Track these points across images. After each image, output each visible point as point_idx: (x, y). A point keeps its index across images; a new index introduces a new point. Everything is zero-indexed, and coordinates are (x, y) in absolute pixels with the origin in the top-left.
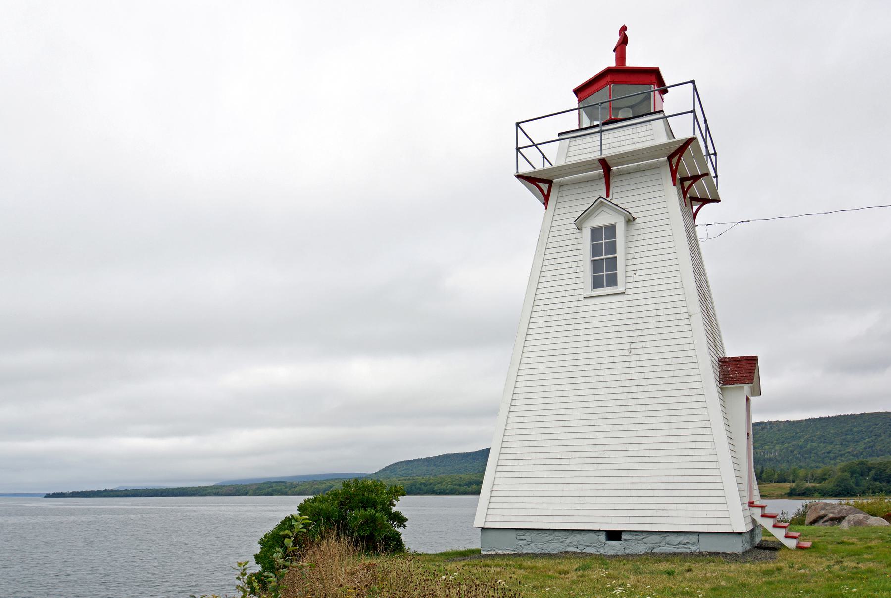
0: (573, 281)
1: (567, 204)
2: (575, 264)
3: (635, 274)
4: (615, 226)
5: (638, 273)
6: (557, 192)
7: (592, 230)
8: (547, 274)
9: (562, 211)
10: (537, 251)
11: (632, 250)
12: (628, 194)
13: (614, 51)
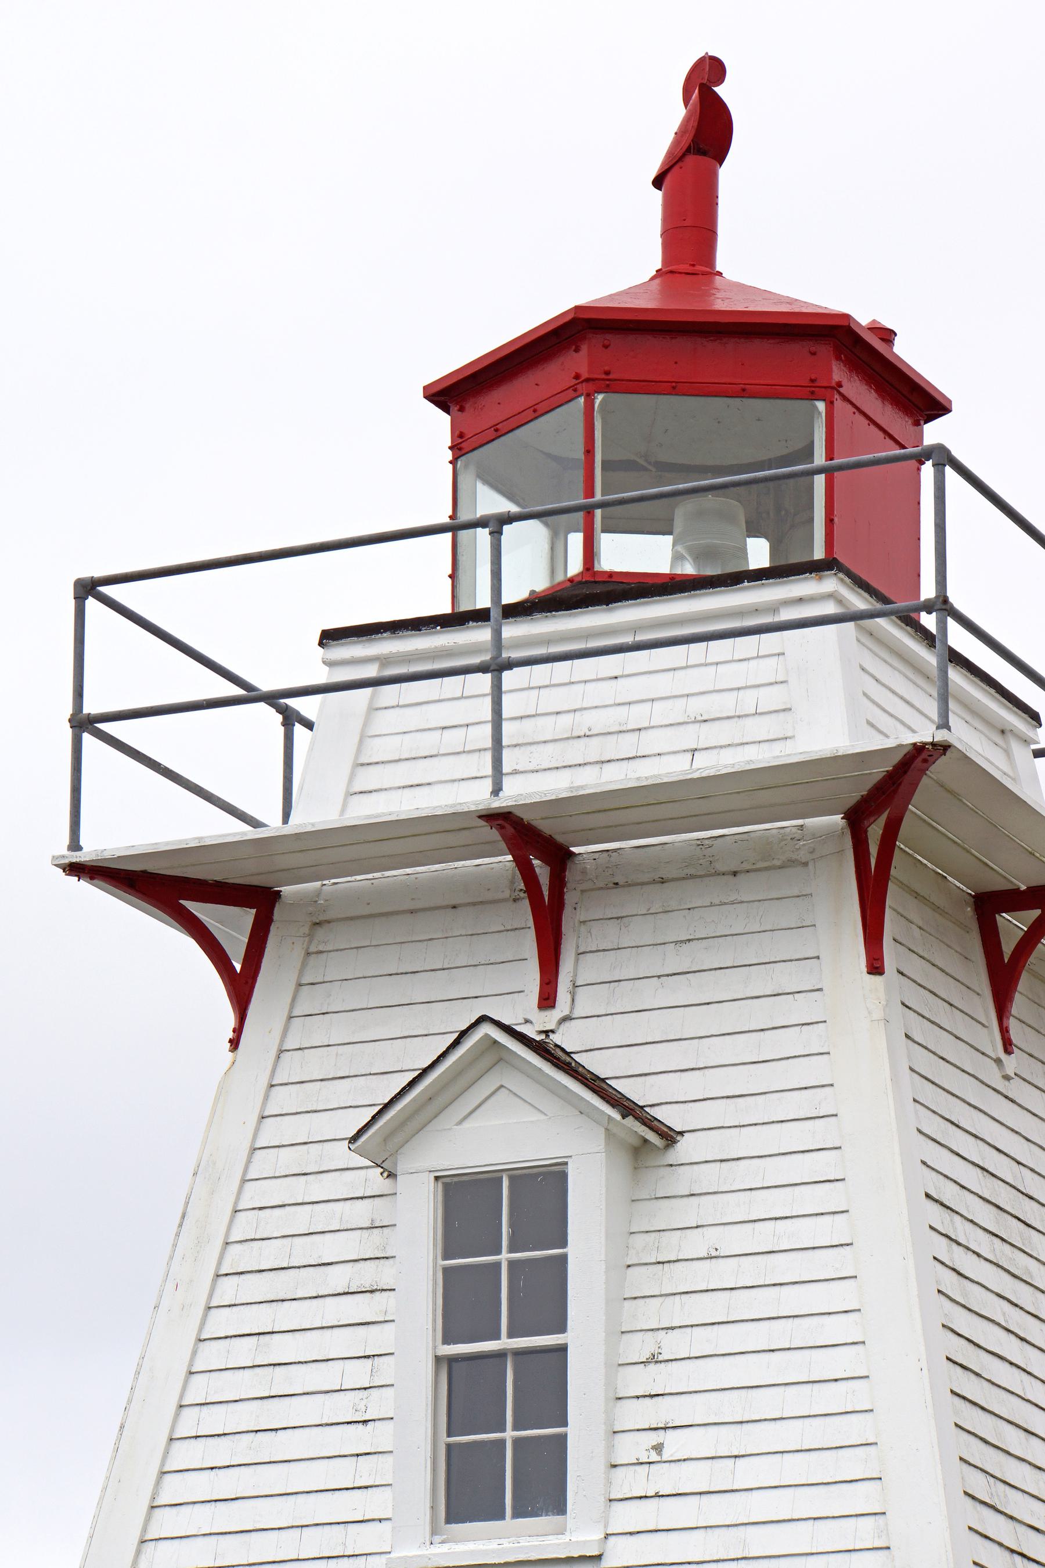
0: (343, 1473)
1: (338, 1030)
2: (358, 1374)
3: (658, 1448)
4: (563, 1177)
5: (675, 1444)
6: (298, 953)
7: (447, 1188)
8: (214, 1420)
9: (316, 1064)
10: (170, 1286)
11: (650, 1314)
12: (650, 994)
13: (658, 183)
